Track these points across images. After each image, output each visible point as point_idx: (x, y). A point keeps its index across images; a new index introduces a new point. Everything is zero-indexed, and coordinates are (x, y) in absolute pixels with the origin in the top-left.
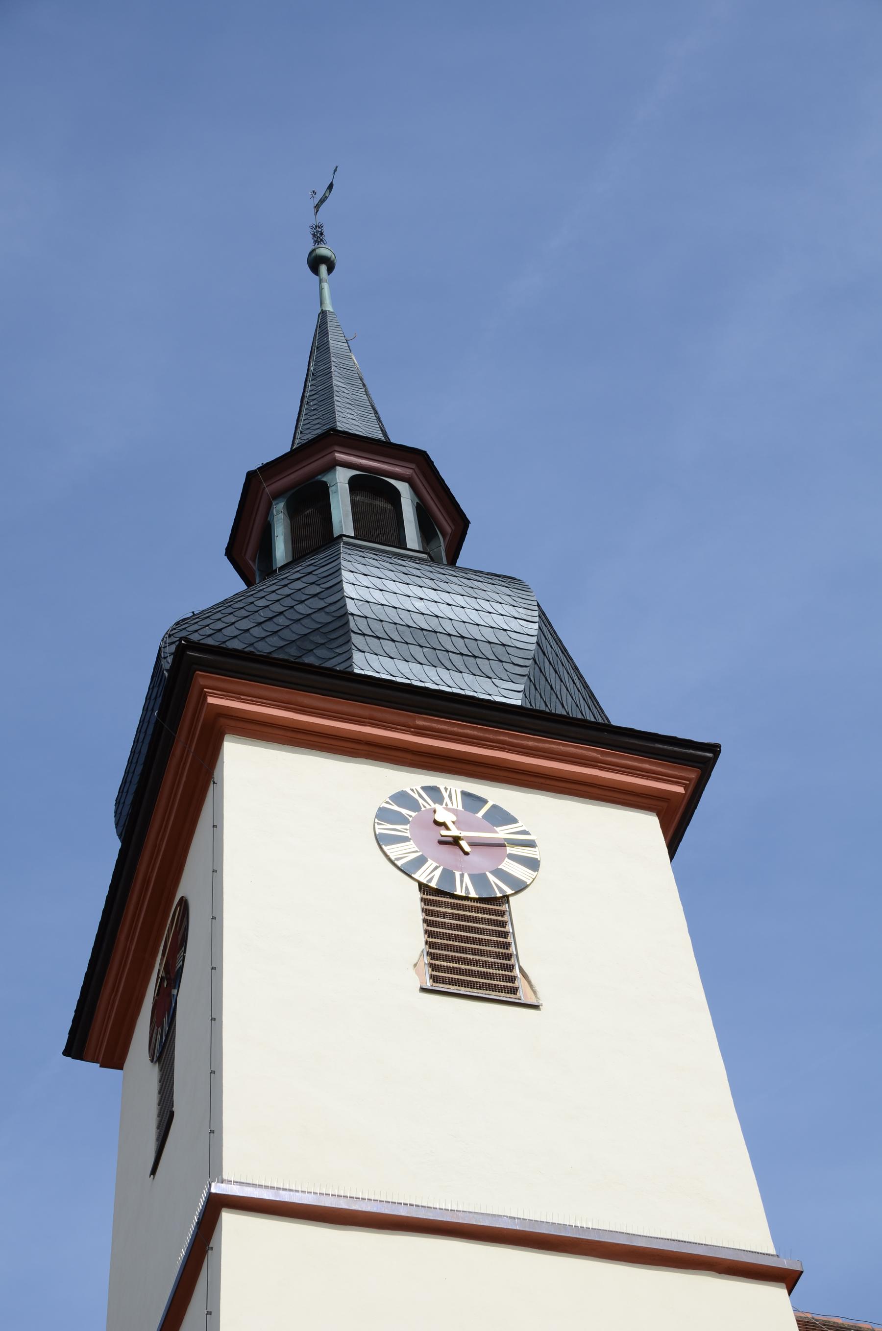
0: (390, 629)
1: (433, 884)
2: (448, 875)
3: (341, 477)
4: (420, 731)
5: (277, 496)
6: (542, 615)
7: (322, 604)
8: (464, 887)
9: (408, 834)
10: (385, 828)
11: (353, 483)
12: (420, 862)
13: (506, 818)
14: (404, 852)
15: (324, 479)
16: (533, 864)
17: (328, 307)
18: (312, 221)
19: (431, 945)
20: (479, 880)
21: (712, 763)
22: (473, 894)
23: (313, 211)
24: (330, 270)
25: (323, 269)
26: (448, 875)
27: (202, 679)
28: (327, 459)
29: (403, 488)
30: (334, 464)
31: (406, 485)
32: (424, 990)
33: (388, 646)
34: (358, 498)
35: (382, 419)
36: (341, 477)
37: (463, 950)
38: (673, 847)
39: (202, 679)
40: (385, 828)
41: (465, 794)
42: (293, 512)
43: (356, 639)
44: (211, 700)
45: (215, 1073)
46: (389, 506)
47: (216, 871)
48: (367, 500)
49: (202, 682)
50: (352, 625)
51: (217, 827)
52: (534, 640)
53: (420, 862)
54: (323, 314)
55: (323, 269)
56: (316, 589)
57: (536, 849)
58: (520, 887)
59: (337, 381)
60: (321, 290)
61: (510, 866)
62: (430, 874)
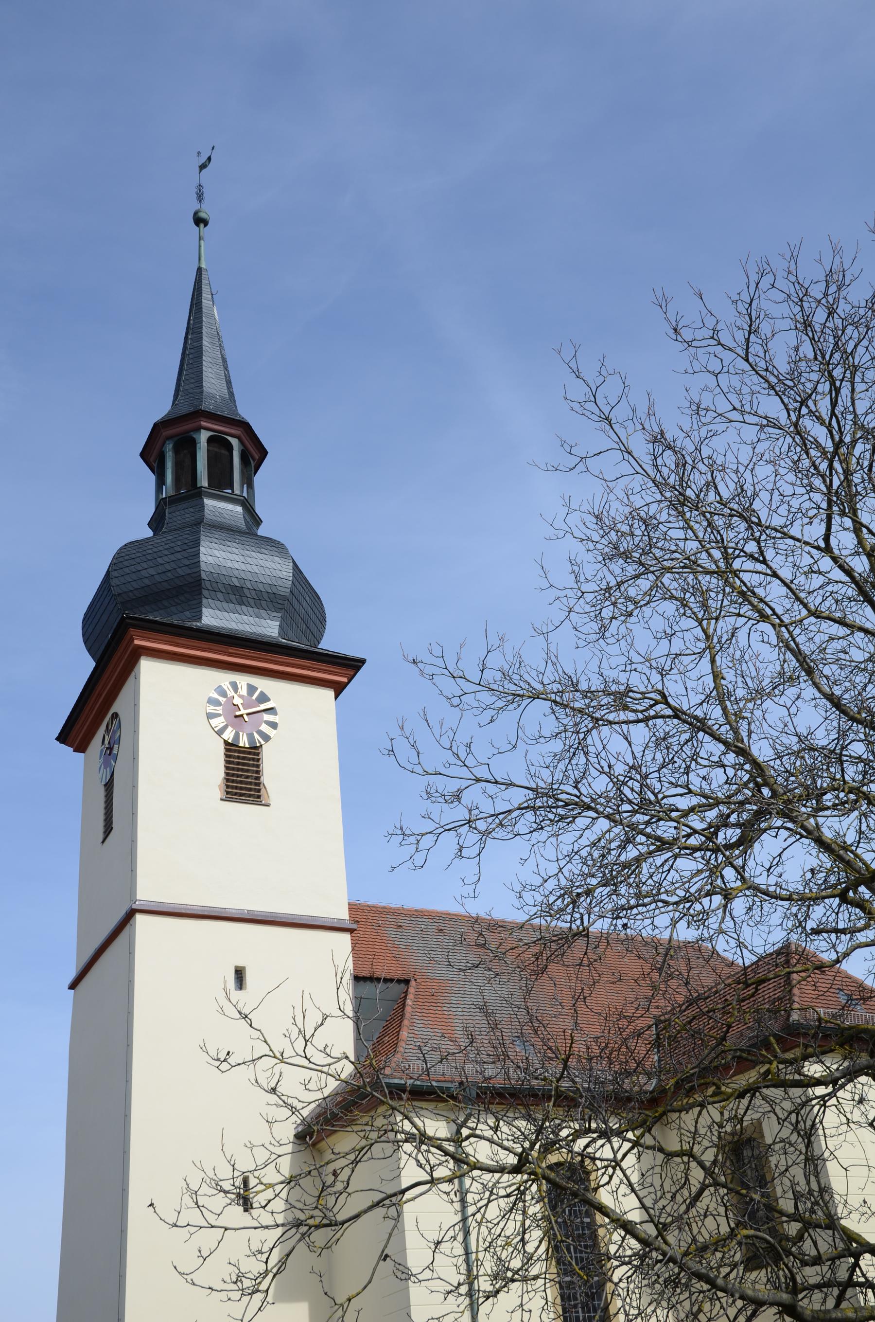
0: (220, 586)
1: (230, 741)
2: (237, 736)
3: (204, 437)
4: (230, 655)
5: (169, 438)
6: (294, 562)
7: (188, 563)
8: (244, 742)
9: (221, 712)
10: (211, 709)
11: (210, 440)
12: (225, 728)
13: (263, 698)
14: (218, 722)
15: (194, 436)
16: (274, 725)
17: (203, 266)
18: (196, 206)
19: (228, 786)
20: (251, 737)
21: (358, 669)
22: (247, 746)
23: (198, 169)
24: (206, 225)
25: (202, 225)
26: (237, 736)
27: (132, 631)
28: (197, 424)
29: (234, 442)
30: (198, 429)
31: (236, 440)
32: (222, 800)
33: (220, 595)
34: (211, 448)
35: (230, 369)
36: (204, 437)
37: (240, 776)
38: (336, 698)
39: (132, 631)
40: (211, 709)
41: (248, 685)
42: (177, 450)
43: (205, 592)
44: (136, 642)
45: (134, 787)
46: (227, 453)
47: (136, 705)
48: (216, 450)
49: (132, 633)
50: (203, 586)
51: (137, 678)
52: (288, 590)
53: (225, 728)
54: (200, 270)
55: (202, 225)
56: (187, 562)
57: (275, 731)
58: (267, 738)
59: (206, 342)
60: (200, 246)
61: (264, 728)
62: (229, 735)
